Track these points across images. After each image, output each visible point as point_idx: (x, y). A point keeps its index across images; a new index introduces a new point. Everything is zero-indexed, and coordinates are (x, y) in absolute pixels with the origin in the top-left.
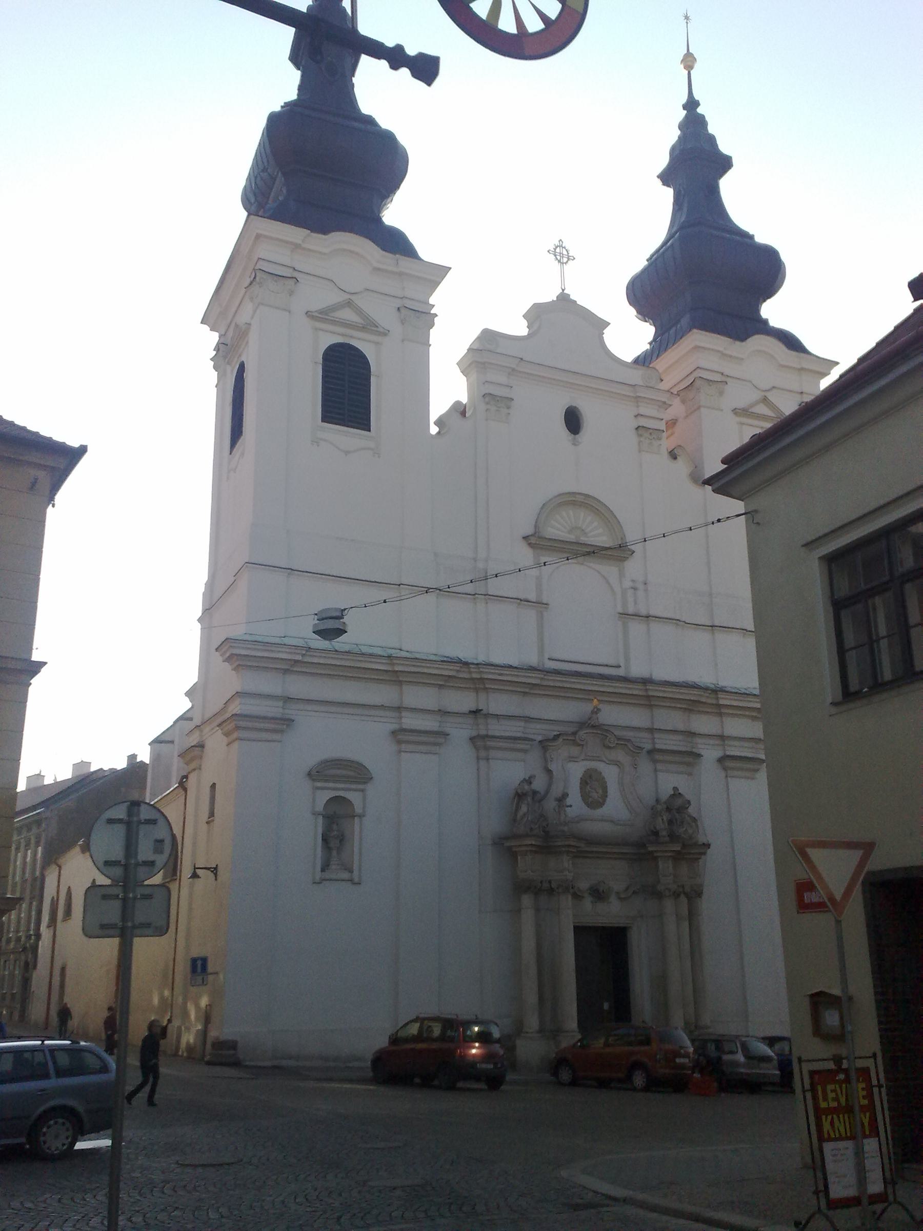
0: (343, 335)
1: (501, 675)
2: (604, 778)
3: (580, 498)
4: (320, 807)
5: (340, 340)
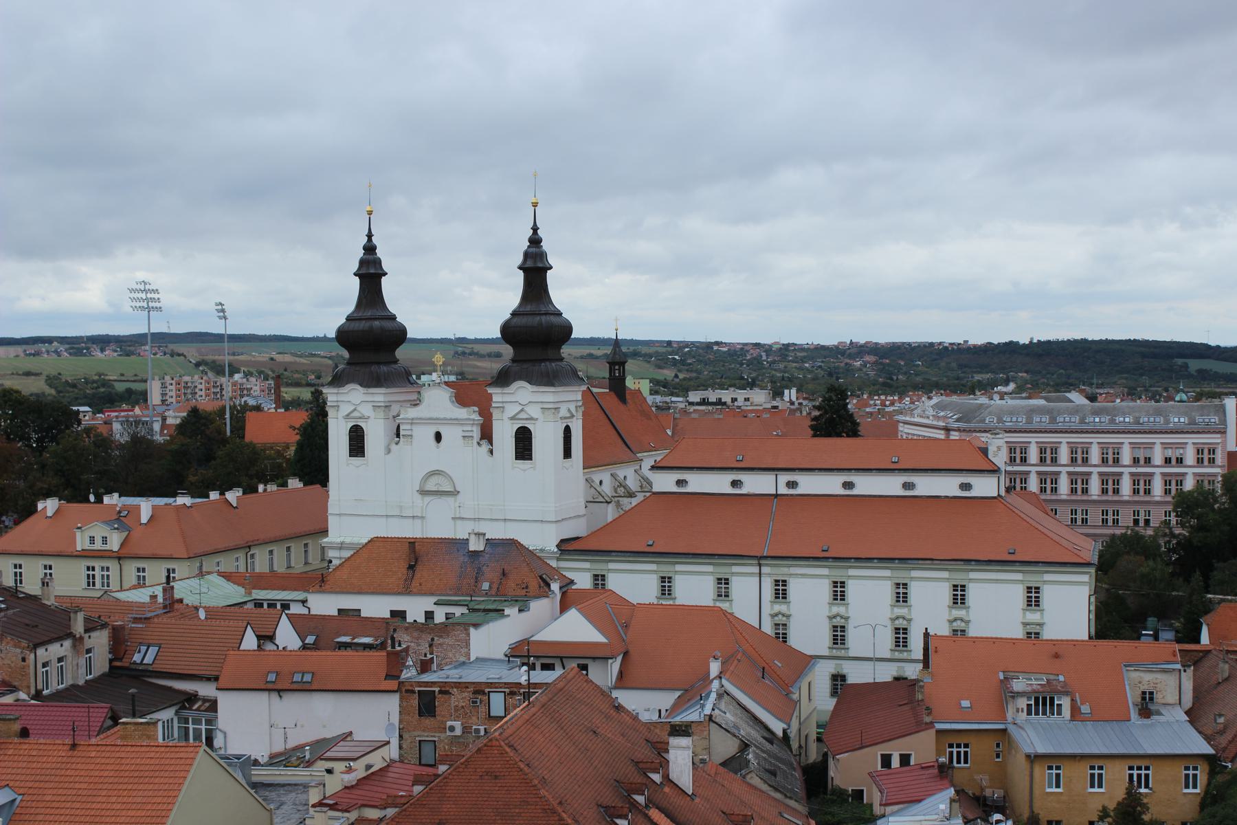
3: (437, 472)
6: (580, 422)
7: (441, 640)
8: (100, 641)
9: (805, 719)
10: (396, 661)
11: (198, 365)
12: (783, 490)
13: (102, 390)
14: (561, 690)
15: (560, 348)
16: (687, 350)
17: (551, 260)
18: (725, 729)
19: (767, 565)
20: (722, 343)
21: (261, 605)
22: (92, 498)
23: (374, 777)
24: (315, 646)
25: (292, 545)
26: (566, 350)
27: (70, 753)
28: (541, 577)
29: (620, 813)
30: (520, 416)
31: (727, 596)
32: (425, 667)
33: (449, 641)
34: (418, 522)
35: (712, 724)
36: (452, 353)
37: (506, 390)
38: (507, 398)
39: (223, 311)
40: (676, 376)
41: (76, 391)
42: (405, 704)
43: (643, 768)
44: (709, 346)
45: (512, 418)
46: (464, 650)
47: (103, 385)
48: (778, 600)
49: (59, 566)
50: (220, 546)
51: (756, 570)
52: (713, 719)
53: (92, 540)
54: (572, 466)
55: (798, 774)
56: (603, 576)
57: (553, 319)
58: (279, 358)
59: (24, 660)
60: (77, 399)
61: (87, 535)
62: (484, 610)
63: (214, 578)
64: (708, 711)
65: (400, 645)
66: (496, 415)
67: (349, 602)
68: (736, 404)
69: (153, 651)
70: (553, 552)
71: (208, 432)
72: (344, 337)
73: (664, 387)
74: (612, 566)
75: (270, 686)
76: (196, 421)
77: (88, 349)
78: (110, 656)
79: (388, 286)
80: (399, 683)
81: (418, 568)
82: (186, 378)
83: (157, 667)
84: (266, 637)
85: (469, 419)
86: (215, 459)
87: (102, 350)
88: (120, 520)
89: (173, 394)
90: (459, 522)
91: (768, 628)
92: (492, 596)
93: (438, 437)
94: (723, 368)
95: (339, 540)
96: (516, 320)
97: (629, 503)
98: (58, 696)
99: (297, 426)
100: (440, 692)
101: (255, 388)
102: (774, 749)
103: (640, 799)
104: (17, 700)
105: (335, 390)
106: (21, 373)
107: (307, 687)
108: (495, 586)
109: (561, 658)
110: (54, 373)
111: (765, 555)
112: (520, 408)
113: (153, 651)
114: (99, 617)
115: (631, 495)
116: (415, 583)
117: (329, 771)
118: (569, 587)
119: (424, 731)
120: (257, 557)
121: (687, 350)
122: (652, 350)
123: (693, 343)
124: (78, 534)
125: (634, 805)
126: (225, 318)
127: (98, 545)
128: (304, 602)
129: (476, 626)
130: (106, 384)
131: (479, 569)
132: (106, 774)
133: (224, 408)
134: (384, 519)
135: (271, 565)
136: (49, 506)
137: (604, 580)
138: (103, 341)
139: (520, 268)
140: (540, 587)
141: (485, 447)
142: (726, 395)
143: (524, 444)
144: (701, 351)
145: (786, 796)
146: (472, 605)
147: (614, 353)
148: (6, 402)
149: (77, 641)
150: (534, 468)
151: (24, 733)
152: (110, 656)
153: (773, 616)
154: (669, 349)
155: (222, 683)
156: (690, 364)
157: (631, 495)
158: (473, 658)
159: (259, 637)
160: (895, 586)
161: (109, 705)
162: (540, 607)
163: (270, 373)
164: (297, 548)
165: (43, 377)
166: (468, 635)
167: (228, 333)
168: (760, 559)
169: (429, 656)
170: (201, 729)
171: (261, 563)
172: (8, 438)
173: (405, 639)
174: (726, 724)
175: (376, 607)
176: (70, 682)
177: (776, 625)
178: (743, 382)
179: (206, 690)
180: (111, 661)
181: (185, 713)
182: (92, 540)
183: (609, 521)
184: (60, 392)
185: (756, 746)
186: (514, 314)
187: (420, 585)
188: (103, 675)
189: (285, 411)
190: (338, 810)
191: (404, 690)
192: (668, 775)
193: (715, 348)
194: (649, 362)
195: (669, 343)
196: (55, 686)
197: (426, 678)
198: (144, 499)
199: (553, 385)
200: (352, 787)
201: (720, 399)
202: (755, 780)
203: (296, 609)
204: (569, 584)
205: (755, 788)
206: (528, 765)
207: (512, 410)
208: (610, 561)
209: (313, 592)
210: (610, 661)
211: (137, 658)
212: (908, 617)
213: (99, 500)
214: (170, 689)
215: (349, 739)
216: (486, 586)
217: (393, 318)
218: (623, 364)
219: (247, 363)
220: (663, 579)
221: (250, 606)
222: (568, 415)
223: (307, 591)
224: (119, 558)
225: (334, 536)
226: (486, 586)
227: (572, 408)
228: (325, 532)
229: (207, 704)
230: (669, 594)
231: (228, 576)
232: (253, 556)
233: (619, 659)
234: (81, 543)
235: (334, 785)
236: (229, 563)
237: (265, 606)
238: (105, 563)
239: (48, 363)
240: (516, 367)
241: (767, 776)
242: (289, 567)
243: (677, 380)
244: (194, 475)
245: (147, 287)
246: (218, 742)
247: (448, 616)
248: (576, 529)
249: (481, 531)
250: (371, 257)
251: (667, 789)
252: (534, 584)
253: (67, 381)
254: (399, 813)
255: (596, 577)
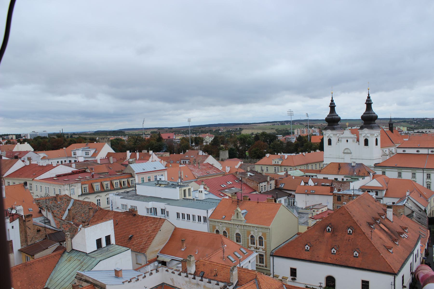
6: (380, 137)
7: (344, 185)
8: (273, 182)
9: (432, 207)
10: (332, 190)
11: (306, 126)
12: (430, 153)
13: (286, 132)
14: (362, 197)
15: (375, 121)
16: (418, 120)
17: (372, 101)
18: (408, 208)
19: (425, 170)
20: (427, 118)
21: (307, 176)
22: (276, 154)
23: (323, 213)
24: (317, 185)
25: (317, 164)
26: (376, 121)
27: (257, 204)
28: (368, 172)
29: (372, 224)
30: (365, 136)
31: (415, 177)
32: (339, 190)
33: (345, 185)
34: (343, 159)
35: (405, 206)
36: (361, 122)
37: (362, 131)
38: (362, 132)
39: (307, 115)
40: (415, 126)
41: (281, 132)
42: (334, 198)
43: (380, 215)
44: (424, 119)
45: (364, 137)
46: (349, 187)
47: (287, 131)
48: (428, 179)
49: (269, 168)
50: (301, 164)
51: (422, 171)
52: (405, 205)
53: (275, 162)
54: (378, 147)
55: (427, 219)
56: (385, 172)
57: (373, 115)
58: (323, 124)
59: (257, 185)
60: (281, 134)
61: (275, 161)
62: (355, 179)
63: (298, 170)
64: (404, 203)
65: (333, 186)
66: (360, 136)
67: (326, 176)
68: (426, 132)
69: (283, 185)
70: (373, 167)
71: (302, 140)
72: (327, 120)
73: (412, 129)
74: (387, 170)
75: (306, 193)
76: (300, 138)
77: (284, 123)
78: (275, 185)
79: (373, 106)
80: (333, 194)
81: (340, 169)
82: (302, 129)
83: (284, 188)
84: (306, 183)
85: (354, 137)
86: (304, 146)
87: (287, 124)
88: (282, 158)
89: (299, 132)
90: (352, 159)
91: (425, 186)
92: (357, 176)
93: (347, 141)
94: (427, 124)
95: (326, 163)
96: (365, 115)
97: (392, 155)
98: (264, 193)
99: (321, 139)
100: (342, 196)
101: (316, 131)
102: (421, 213)
103: (378, 222)
104: (256, 193)
105: (325, 131)
106: (271, 128)
107: (313, 193)
108: (357, 174)
109: (372, 190)
110: (277, 128)
111: (425, 168)
112: (365, 134)
113: (283, 185)
114: (273, 178)
115: (393, 154)
116: (340, 172)
117: (314, 211)
118: (375, 174)
119: (338, 204)
120: (309, 166)
121: (418, 120)
122: (409, 120)
123: (420, 118)
124: (273, 161)
125: (376, 223)
126: (308, 116)
127: (277, 163)
128: (316, 176)
129: (352, 182)
130: (287, 130)
131: (354, 170)
132: (264, 208)
133: (308, 135)
134: (336, 159)
135: (312, 168)
136: (268, 155)
137: (385, 173)
138: (287, 122)
139: (365, 103)
140: (368, 174)
141: (358, 143)
142: (424, 131)
143: (366, 142)
144: (422, 120)
145: (422, 224)
146: (352, 178)
147: (390, 121)
148: (263, 134)
149: (268, 182)
150: (369, 148)
151: (249, 199)
152: (275, 185)
153: (427, 182)
154: (414, 120)
155: (296, 192)
156: (419, 123)
157: (393, 154)
158: (351, 189)
159: (305, 183)
160: (398, 173)
161: (272, 195)
162: (367, 179)
163: (321, 127)
164: (318, 165)
165: (275, 129)
166: (350, 184)
167: (309, 119)
168: (423, 169)
169: (340, 188)
170: (292, 201)
171: (310, 168)
172: (264, 142)
173: (335, 184)
174: (409, 206)
175: (331, 177)
176: (267, 190)
177: (427, 184)
178: (432, 127)
179: (293, 193)
180: (275, 186)
181: (289, 198)
182: (275, 162)
183: (388, 159)
184: (278, 132)
185: (416, 212)
186: (364, 114)
187: (341, 173)
188: (274, 189)
189: (96, 143)
190: (314, 219)
191: (334, 195)
192: (386, 217)
193: (425, 119)
194: (408, 123)
195: (414, 119)
196: (264, 191)
197: (339, 193)
198: (286, 154)
199: (373, 129)
200: (318, 215)
201: (422, 131)
202: (414, 220)
203: (314, 177)
204: (375, 173)
205: (414, 221)
206: (350, 212)
207: (364, 135)
208: (386, 169)
209: (318, 174)
210: (383, 191)
211: (280, 186)
212: (416, 181)
213: (277, 154)
214: (286, 193)
215: (321, 205)
216: (355, 173)
217: (338, 115)
218: (392, 124)
219: (316, 126)
220: (399, 173)
221: (305, 176)
222: (377, 136)
223: (317, 173)
224: (281, 166)
225: (325, 162)
226: (355, 173)
227: (378, 134)
228: (323, 161)
229: (293, 196)
230: (401, 176)
231: (301, 170)
232: (308, 166)
233: (385, 191)
234: (273, 163)
235: (314, 214)
236: (303, 168)
237: (308, 176)
238: (278, 167)
239: (276, 127)
240: (364, 125)
241: (418, 219)
242: (316, 168)
243: (415, 127)
244: (300, 149)
245: (291, 111)
246: (295, 204)
247: (347, 180)
248: (380, 161)
249: (354, 161)
250: (332, 103)
251: (386, 220)
252: (366, 173)
253: (279, 130)
254: (322, 221)
255: (383, 172)
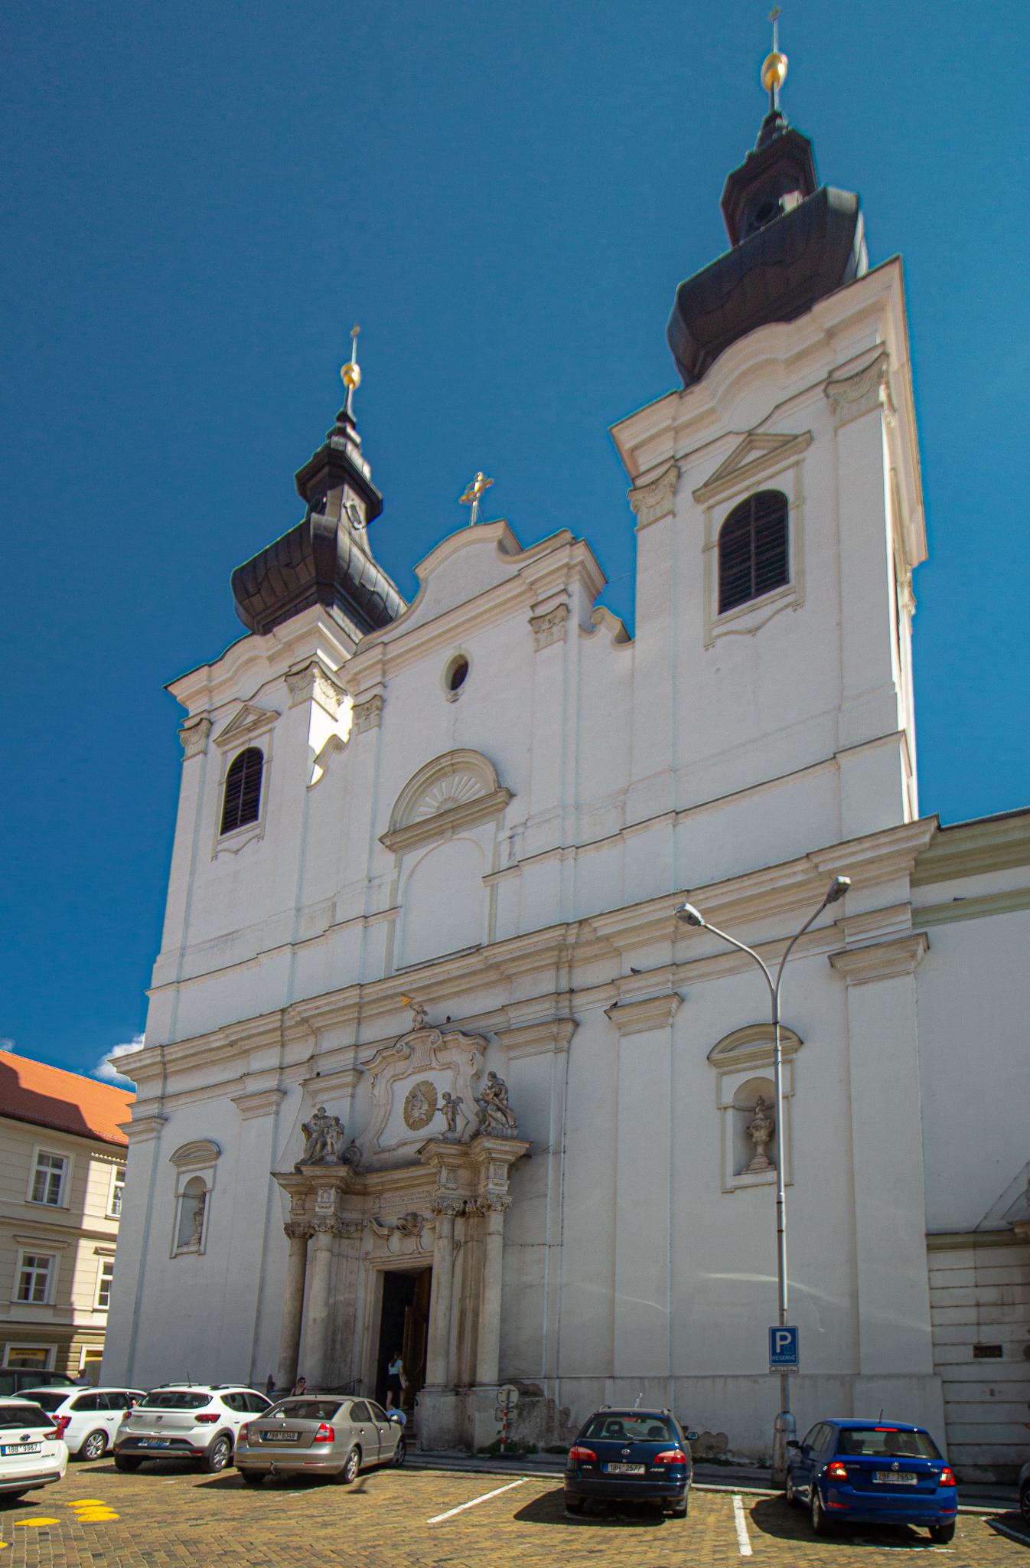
0: (239, 746)
1: (318, 1008)
2: (434, 1089)
3: (445, 762)
4: (728, 1098)
5: (242, 749)
